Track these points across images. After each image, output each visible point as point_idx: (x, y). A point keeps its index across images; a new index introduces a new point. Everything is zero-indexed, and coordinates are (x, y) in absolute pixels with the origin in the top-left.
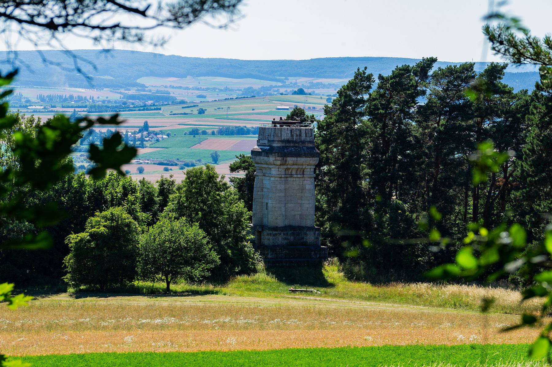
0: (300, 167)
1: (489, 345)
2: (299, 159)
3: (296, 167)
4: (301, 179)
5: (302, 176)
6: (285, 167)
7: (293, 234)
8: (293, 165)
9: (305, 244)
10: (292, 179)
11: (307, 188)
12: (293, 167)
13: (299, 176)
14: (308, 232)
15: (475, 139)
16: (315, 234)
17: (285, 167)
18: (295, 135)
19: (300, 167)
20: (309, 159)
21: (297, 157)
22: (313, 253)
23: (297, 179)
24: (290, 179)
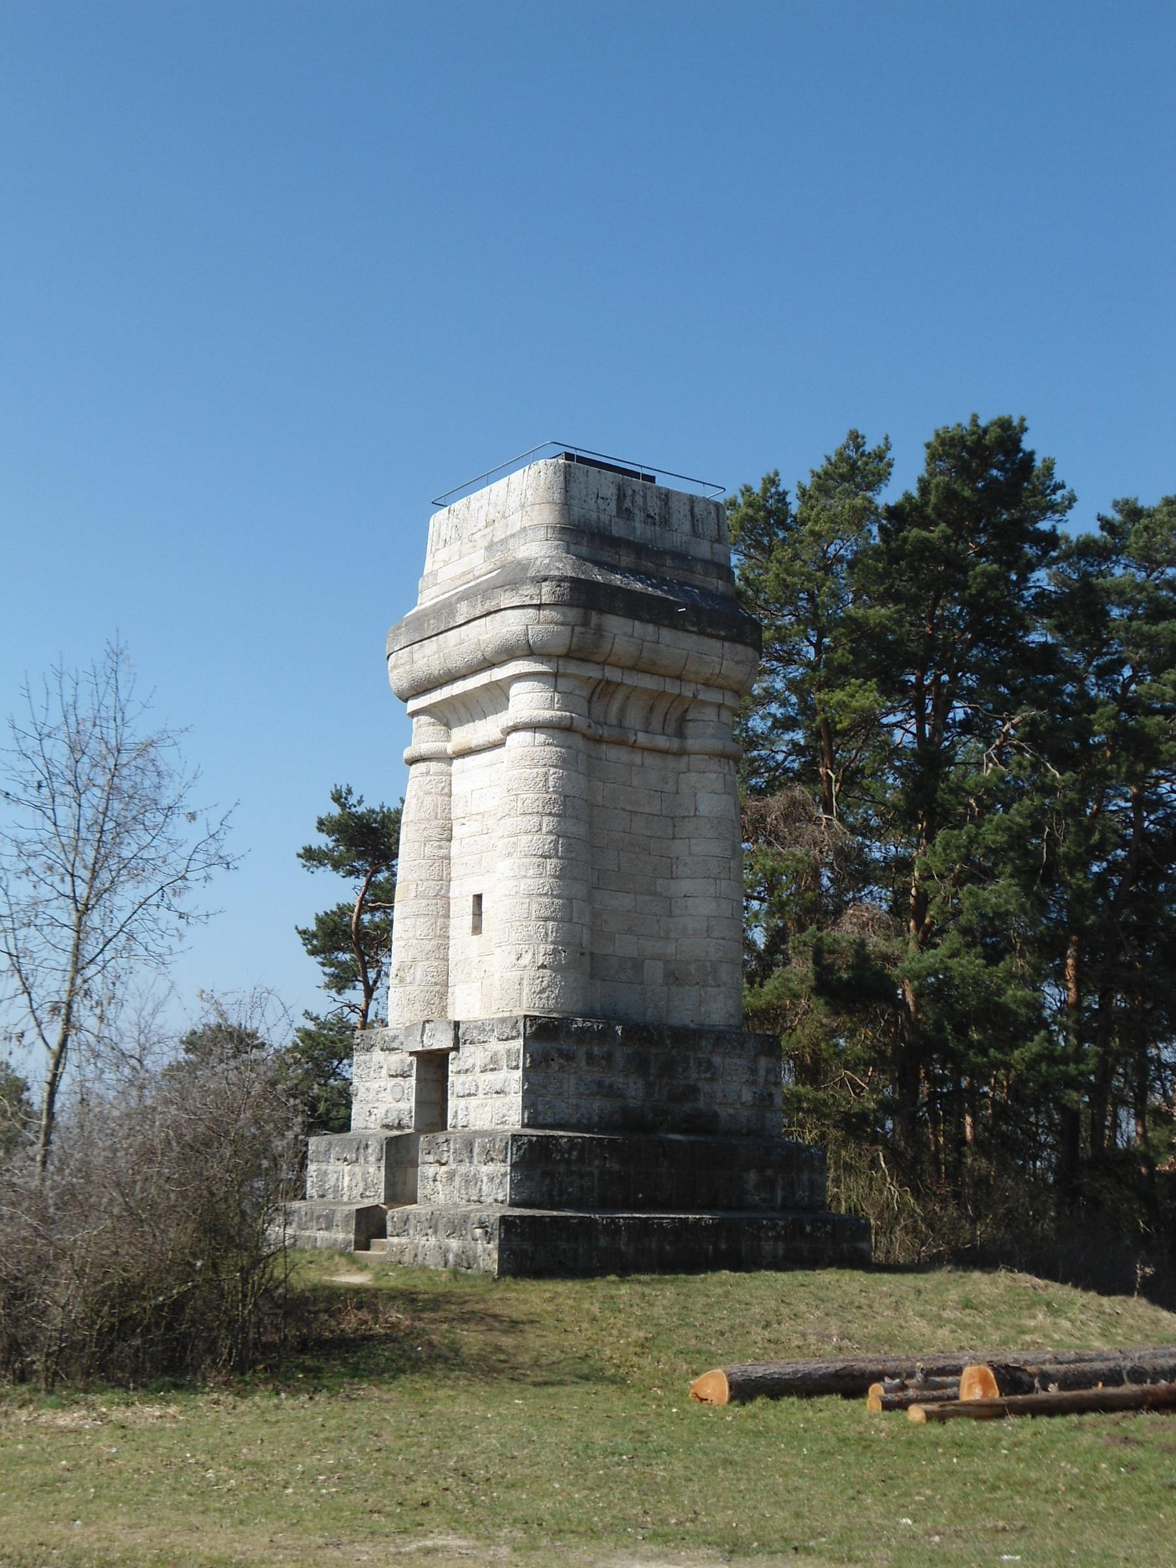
0: (671, 687)
1: (779, 1058)
2: (667, 634)
3: (648, 682)
4: (671, 762)
5: (675, 744)
6: (594, 672)
7: (640, 1065)
8: (635, 668)
9: (702, 1124)
10: (623, 755)
11: (703, 809)
12: (632, 679)
13: (662, 742)
14: (717, 1060)
15: (1125, 686)
16: (754, 1071)
17: (594, 672)
18: (639, 515)
19: (671, 687)
20: (716, 644)
21: (658, 623)
22: (752, 1177)
23: (650, 760)
24: (613, 753)
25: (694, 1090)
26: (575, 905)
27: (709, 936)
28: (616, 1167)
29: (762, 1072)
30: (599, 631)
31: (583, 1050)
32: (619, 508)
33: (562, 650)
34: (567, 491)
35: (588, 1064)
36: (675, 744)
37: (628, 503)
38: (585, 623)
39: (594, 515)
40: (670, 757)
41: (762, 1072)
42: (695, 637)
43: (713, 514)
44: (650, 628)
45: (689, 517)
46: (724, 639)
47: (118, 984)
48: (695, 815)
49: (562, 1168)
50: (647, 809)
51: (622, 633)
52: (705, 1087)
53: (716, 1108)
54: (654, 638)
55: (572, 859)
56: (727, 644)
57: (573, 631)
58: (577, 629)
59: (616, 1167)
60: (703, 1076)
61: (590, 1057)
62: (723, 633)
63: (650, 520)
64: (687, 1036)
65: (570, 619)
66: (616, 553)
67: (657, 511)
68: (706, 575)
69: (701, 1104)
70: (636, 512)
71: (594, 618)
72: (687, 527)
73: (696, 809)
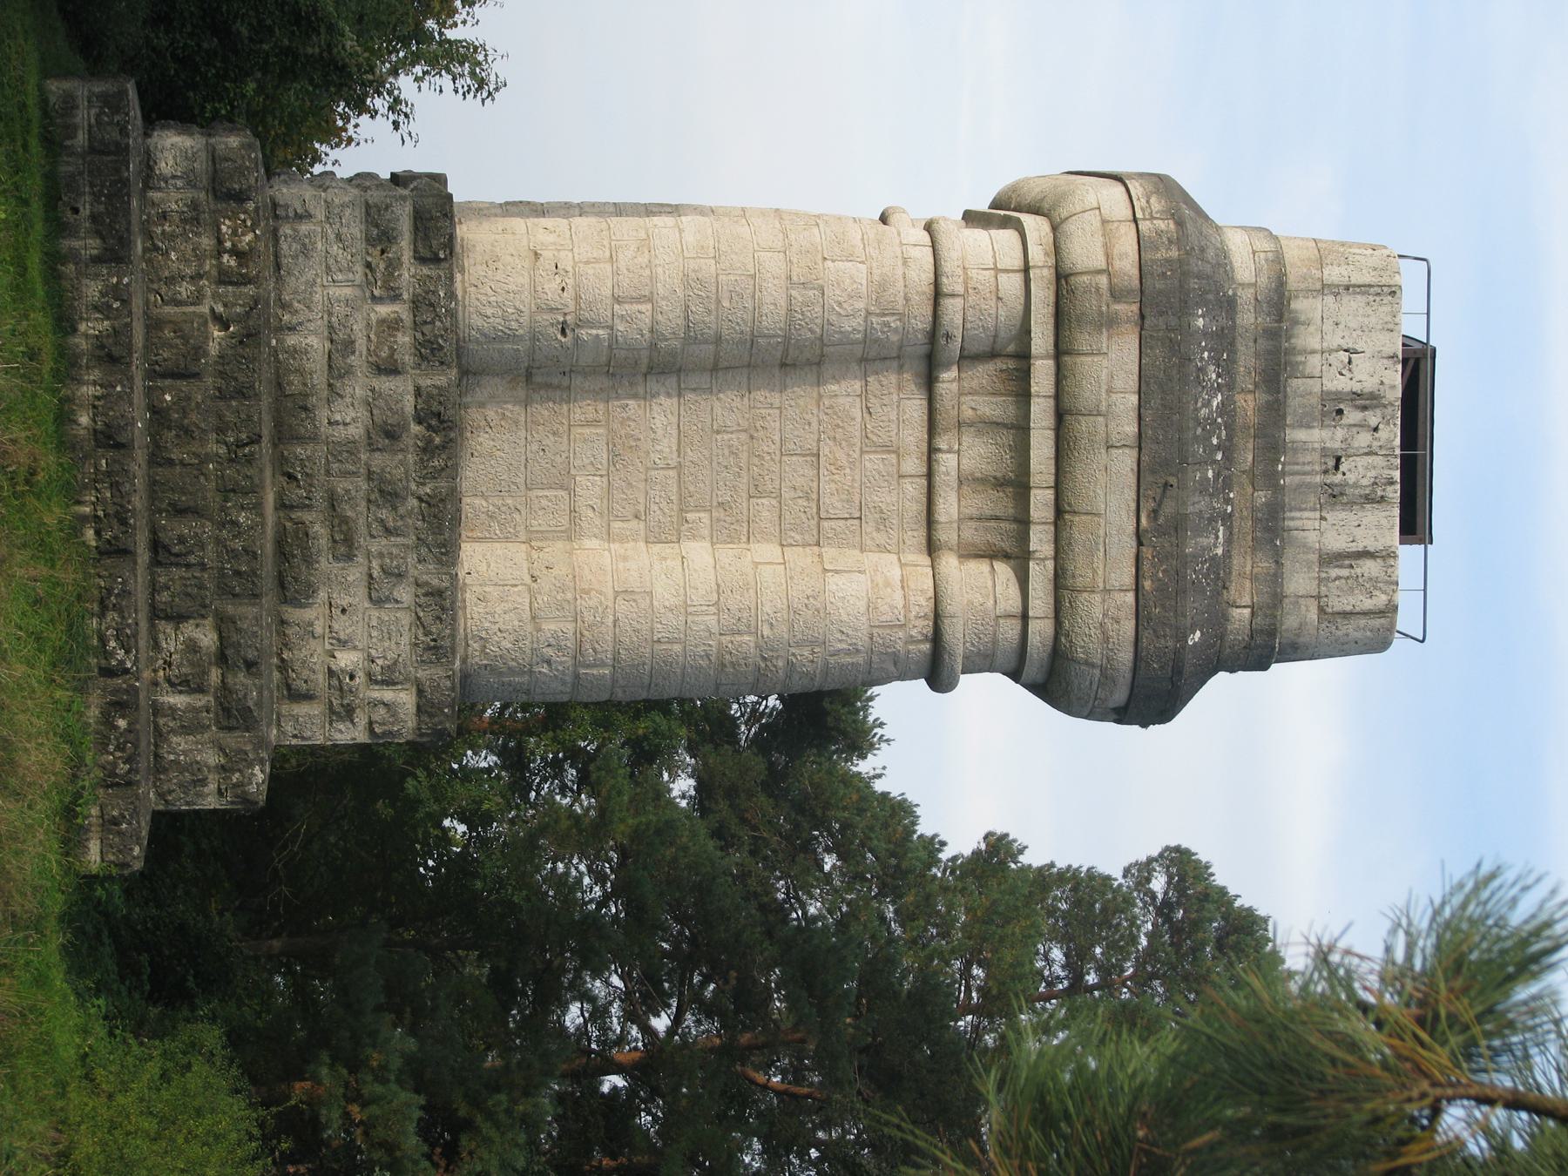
2: (1125, 461)
4: (918, 536)
6: (1041, 339)
10: (913, 435)
16: (388, 680)
23: (914, 489)
25: (345, 546)
26: (643, 307)
27: (617, 594)
28: (213, 349)
29: (388, 695)
30: (1110, 322)
31: (400, 310)
32: (1338, 396)
33: (1067, 265)
34: (1347, 288)
35: (382, 322)
36: (946, 535)
37: (1352, 416)
38: (1116, 294)
39: (1314, 342)
40: (923, 532)
41: (388, 695)
42: (1131, 528)
43: (1368, 604)
44: (1131, 429)
45: (1354, 547)
46: (1138, 589)
47: (528, 580)
48: (826, 570)
49: (206, 242)
50: (827, 488)
51: (1113, 369)
52: (355, 574)
53: (322, 595)
54: (1114, 439)
55: (718, 302)
56: (1130, 598)
57: (1099, 272)
58: (1103, 280)
59: (213, 349)
60: (375, 564)
61: (392, 325)
62: (1147, 584)
63: (1331, 463)
64: (441, 527)
65: (1117, 264)
66: (1256, 385)
67: (1351, 478)
68: (1254, 578)
69: (325, 564)
70: (1340, 433)
71: (1128, 309)
72: (1336, 542)
73: (837, 572)
